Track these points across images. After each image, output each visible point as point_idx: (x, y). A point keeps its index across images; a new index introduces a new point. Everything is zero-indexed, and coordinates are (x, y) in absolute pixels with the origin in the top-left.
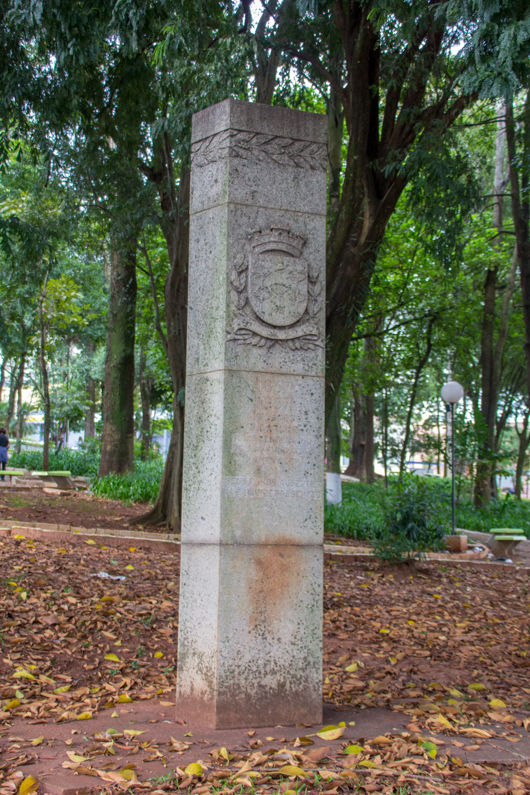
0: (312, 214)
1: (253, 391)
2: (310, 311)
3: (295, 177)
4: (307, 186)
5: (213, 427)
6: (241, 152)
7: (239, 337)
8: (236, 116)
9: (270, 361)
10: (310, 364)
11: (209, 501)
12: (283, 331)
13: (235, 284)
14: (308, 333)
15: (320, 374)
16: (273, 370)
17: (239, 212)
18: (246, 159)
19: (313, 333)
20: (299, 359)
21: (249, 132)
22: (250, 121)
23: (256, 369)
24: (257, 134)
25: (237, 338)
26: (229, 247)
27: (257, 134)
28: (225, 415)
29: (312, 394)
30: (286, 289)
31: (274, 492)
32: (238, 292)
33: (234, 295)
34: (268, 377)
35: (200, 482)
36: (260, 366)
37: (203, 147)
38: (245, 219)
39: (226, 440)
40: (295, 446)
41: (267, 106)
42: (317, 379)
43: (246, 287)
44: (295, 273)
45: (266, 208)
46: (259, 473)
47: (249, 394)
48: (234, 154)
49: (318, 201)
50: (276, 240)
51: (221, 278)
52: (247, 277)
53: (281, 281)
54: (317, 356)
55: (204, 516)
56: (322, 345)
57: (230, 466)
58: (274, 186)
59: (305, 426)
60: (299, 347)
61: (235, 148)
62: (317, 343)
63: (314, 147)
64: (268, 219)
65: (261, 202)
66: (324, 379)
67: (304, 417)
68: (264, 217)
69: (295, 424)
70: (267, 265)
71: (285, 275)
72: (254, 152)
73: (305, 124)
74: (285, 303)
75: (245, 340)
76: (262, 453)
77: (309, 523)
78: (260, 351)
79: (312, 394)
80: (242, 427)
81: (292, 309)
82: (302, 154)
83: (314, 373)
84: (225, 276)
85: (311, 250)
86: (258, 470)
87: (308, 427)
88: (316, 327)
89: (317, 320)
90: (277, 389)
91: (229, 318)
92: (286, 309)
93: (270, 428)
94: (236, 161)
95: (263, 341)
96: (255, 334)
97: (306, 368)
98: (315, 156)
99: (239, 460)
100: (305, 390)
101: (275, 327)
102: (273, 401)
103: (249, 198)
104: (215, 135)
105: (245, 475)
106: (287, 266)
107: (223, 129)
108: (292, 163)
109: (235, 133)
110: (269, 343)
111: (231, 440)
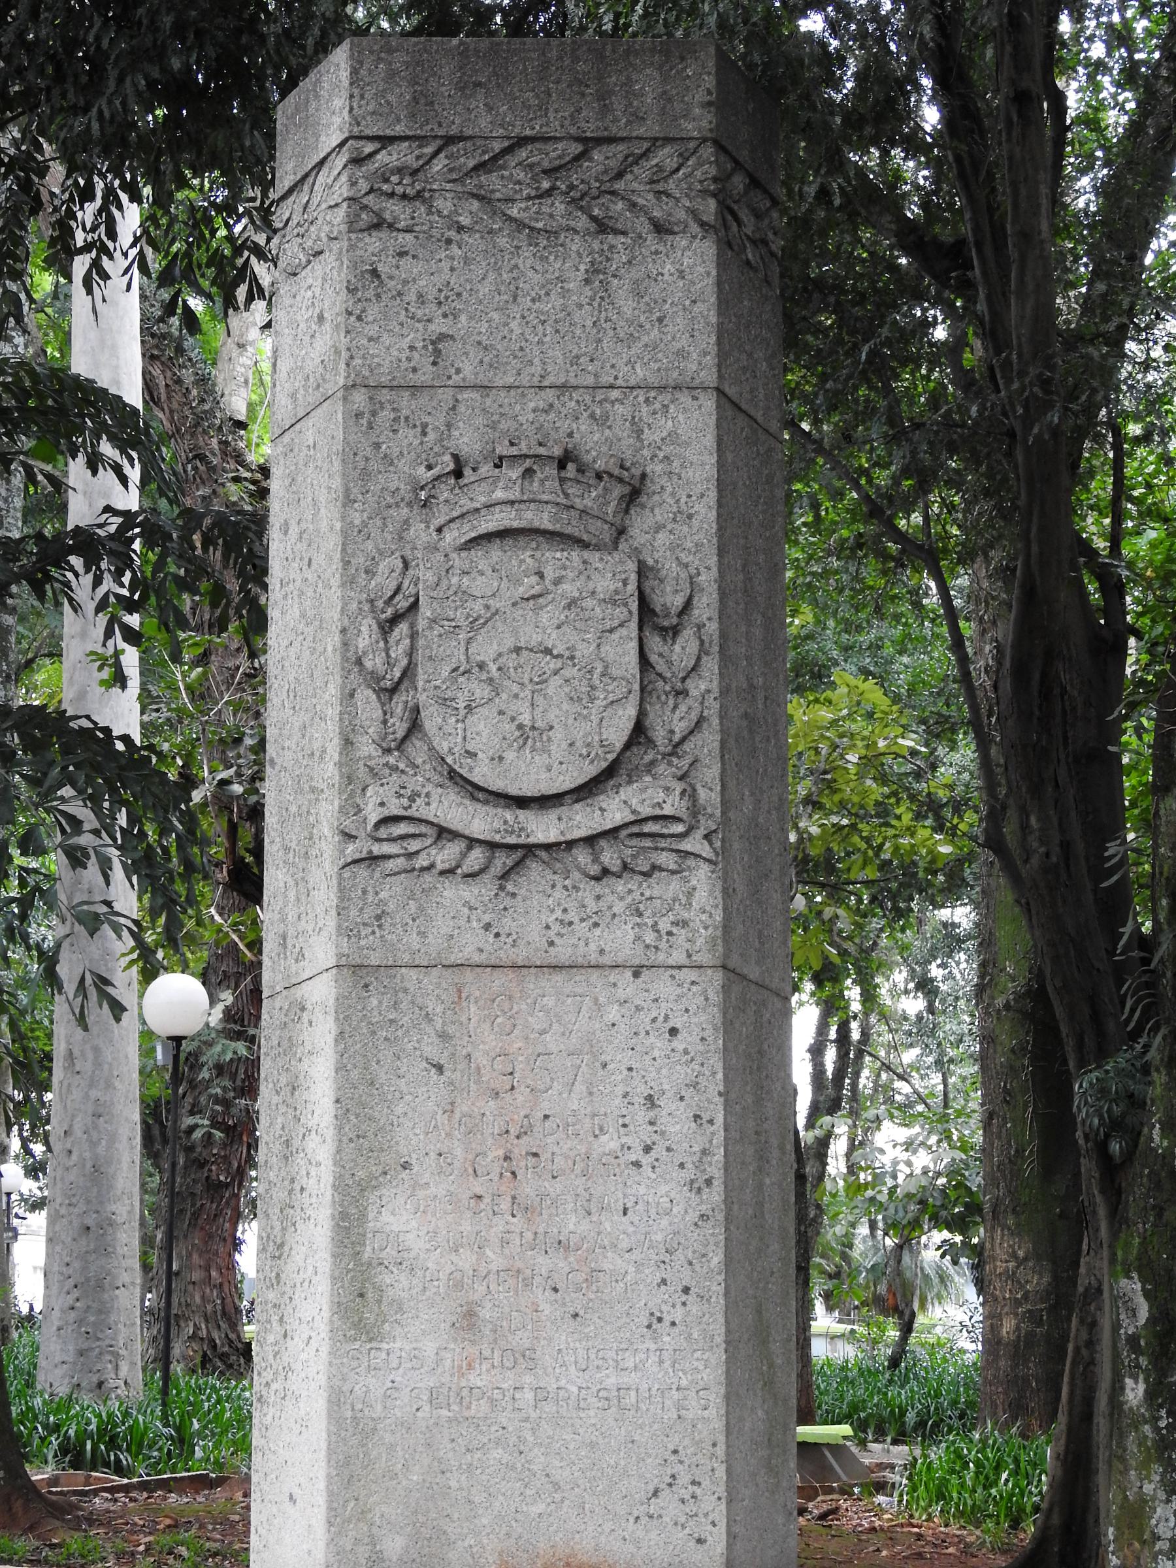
0: (662, 388)
1: (444, 1036)
2: (659, 735)
3: (595, 270)
4: (638, 294)
6: (393, 209)
7: (386, 848)
8: (369, 93)
10: (664, 925)
12: (553, 814)
13: (368, 664)
14: (647, 811)
15: (703, 958)
16: (521, 954)
17: (386, 415)
18: (408, 230)
19: (667, 810)
20: (619, 908)
21: (422, 140)
22: (422, 102)
23: (456, 957)
24: (450, 140)
25: (388, 846)
26: (350, 537)
27: (450, 140)
28: (340, 1128)
29: (673, 1032)
30: (554, 664)
31: (529, 1395)
32: (379, 691)
33: (368, 704)
34: (500, 981)
35: (288, 1369)
36: (472, 944)
37: (298, 208)
38: (408, 436)
39: (344, 1215)
40: (611, 1223)
41: (484, 43)
42: (692, 975)
43: (408, 672)
44: (589, 603)
45: (484, 388)
46: (471, 1327)
47: (432, 1049)
48: (367, 220)
49: (683, 341)
50: (514, 494)
51: (330, 649)
52: (414, 636)
53: (535, 639)
54: (690, 894)
55: (296, 1492)
57: (361, 1308)
58: (515, 311)
59: (647, 1149)
60: (615, 866)
61: (370, 200)
62: (686, 845)
63: (666, 156)
64: (493, 426)
65: (468, 369)
67: (641, 1115)
68: (479, 421)
69: (610, 1143)
70: (479, 585)
71: (550, 615)
72: (439, 203)
73: (629, 82)
74: (551, 716)
77: (668, 1504)
79: (673, 1032)
81: (580, 731)
82: (619, 186)
83: (678, 957)
84: (337, 638)
85: (659, 516)
86: (469, 1319)
87: (659, 1151)
88: (678, 787)
89: (685, 763)
91: (352, 784)
92: (557, 734)
93: (516, 1162)
94: (373, 242)
96: (444, 833)
97: (649, 937)
98: (671, 185)
99: (396, 1283)
100: (645, 1018)
101: (522, 802)
103: (423, 360)
104: (322, 163)
105: (419, 1341)
106: (557, 582)
107: (335, 141)
108: (582, 222)
109: (369, 148)
110: (502, 861)
111: (363, 1217)
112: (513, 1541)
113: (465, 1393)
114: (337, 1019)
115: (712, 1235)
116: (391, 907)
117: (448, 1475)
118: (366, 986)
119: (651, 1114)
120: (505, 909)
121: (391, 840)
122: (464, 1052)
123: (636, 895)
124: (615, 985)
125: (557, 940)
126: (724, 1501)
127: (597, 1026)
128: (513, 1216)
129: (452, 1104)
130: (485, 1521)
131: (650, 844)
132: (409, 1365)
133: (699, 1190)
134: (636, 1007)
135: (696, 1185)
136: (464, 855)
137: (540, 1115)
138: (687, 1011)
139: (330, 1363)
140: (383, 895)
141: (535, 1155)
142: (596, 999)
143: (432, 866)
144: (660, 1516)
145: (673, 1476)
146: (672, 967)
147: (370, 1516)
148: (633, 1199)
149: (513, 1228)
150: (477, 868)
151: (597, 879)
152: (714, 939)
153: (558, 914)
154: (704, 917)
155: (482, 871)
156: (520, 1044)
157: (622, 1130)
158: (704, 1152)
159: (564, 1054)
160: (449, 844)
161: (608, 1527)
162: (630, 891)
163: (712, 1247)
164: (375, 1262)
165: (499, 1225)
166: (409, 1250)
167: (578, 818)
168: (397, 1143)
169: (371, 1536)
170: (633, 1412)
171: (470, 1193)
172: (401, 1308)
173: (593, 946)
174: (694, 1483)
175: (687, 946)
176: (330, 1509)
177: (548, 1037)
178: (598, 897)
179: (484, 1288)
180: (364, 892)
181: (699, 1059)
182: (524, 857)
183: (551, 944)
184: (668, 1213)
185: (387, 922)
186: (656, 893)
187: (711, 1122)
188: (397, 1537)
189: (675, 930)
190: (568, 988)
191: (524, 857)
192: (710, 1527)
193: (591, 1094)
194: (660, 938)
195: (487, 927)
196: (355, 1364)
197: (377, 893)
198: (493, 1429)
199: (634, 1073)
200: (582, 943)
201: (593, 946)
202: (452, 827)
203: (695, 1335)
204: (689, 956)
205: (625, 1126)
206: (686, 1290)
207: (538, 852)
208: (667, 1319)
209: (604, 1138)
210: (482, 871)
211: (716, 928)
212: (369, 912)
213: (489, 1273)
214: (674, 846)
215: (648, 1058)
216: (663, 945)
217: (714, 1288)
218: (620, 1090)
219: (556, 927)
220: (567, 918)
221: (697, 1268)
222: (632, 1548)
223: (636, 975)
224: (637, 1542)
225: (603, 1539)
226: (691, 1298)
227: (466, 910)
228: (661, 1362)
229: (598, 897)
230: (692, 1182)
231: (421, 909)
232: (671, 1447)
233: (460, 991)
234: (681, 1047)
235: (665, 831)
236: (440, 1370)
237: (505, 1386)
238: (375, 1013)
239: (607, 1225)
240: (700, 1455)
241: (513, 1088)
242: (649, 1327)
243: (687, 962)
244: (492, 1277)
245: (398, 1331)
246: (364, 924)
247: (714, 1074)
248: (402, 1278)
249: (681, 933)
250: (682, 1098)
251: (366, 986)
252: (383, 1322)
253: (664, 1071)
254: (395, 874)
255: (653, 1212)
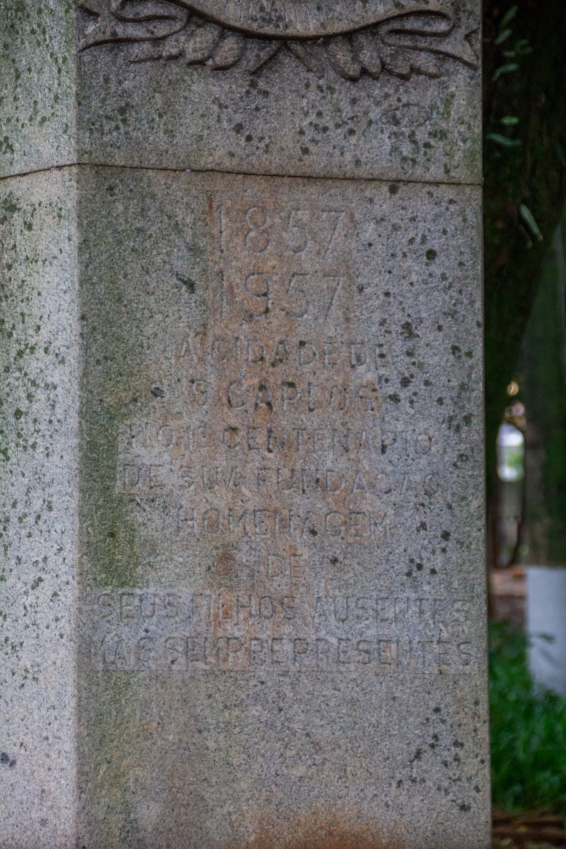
1: (194, 250)
5: (41, 395)
7: (132, 31)
9: (259, 126)
10: (422, 136)
11: (31, 688)
16: (274, 162)
20: (375, 113)
23: (207, 161)
28: (86, 348)
29: (431, 254)
31: (288, 647)
34: (253, 190)
36: (222, 148)
42: (449, 193)
46: (227, 571)
54: (449, 100)
56: (470, 52)
59: (405, 382)
62: (446, 47)
66: (478, 194)
67: (400, 346)
69: (366, 374)
75: (157, 41)
76: (237, 493)
77: (431, 768)
78: (219, 88)
79: (431, 254)
80: (157, 393)
83: (436, 172)
87: (417, 385)
90: (291, 237)
95: (230, 47)
97: (406, 149)
99: (150, 523)
102: (274, 287)
105: (174, 582)
110: (255, 54)
111: (112, 446)
112: (273, 806)
113: (222, 643)
114: (80, 225)
115: (471, 476)
116: (136, 99)
117: (205, 734)
118: (111, 188)
119: (410, 344)
120: (257, 109)
121: (137, 21)
122: (216, 269)
123: (393, 100)
124: (371, 200)
125: (312, 148)
126: (487, 764)
127: (354, 245)
128: (270, 451)
129: (204, 326)
130: (244, 786)
131: (409, 43)
132: (163, 613)
133: (458, 429)
134: (393, 226)
135: (455, 423)
136: (216, 45)
137: (295, 341)
138: (445, 232)
139: (79, 609)
140: (127, 84)
141: (291, 385)
142: (352, 216)
143: (181, 54)
144: (423, 780)
145: (435, 737)
146: (430, 183)
147: (123, 780)
148: (391, 436)
149: (269, 464)
150: (231, 60)
151: (353, 80)
152: (472, 153)
153: (313, 117)
154: (462, 129)
155: (235, 64)
156: (274, 262)
157: (379, 360)
158: (463, 387)
159: (320, 275)
160: (200, 31)
161: (370, 791)
162: (387, 96)
163: (471, 490)
164: (126, 498)
165: (255, 461)
166: (162, 486)
167: (338, 8)
168: (147, 366)
169: (126, 803)
170: (393, 667)
171: (224, 425)
172: (154, 550)
173: (348, 157)
174: (457, 744)
175: (445, 160)
176: (80, 773)
177: (303, 254)
178: (354, 101)
179: (241, 529)
180: (107, 80)
181: (457, 286)
182: (278, 51)
183: (306, 151)
184: (426, 451)
185: (131, 116)
186: (413, 98)
187: (469, 354)
188: (152, 804)
189: (432, 142)
190: (323, 202)
191: (278, 51)
192: (473, 793)
193: (347, 320)
194: (417, 150)
195: (239, 128)
196: (106, 611)
197: (120, 83)
198: (252, 683)
199: (391, 299)
200: (337, 152)
201: (348, 157)
202: (206, 10)
203: (455, 585)
204: (447, 171)
205: (382, 356)
206: (446, 536)
207: (293, 46)
208: (427, 566)
209: (361, 369)
210: (235, 64)
211: (474, 141)
212: (112, 104)
213: (245, 512)
214: (434, 47)
215: (405, 283)
216: (421, 158)
217: (474, 534)
218: (377, 316)
219: (310, 133)
220: (322, 122)
221: (457, 511)
222: (395, 815)
223: (393, 190)
224: (400, 808)
225: (365, 805)
226: (451, 544)
227: (216, 108)
228: (422, 612)
229: (354, 101)
230: (451, 419)
231: (168, 103)
232: (433, 705)
233: (210, 200)
234: (438, 272)
235: (427, 29)
236: (195, 619)
237: (263, 636)
238: (121, 220)
239: (366, 464)
240: (462, 714)
241: (267, 311)
242: (409, 574)
243: (445, 178)
244: (248, 517)
245: (152, 575)
246: (108, 118)
247: (472, 303)
248: (155, 517)
249: (439, 145)
250: (440, 328)
251: (111, 188)
252: (136, 565)
253: (421, 298)
254: (140, 62)
255: (411, 450)
